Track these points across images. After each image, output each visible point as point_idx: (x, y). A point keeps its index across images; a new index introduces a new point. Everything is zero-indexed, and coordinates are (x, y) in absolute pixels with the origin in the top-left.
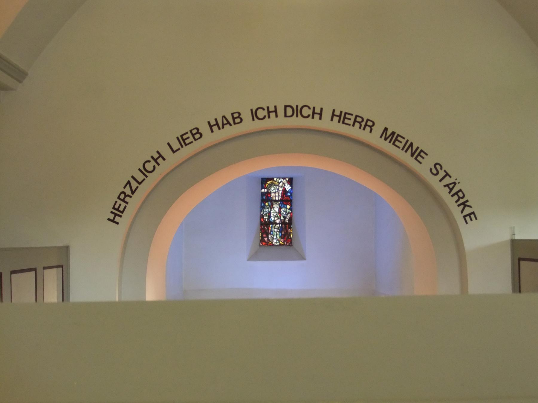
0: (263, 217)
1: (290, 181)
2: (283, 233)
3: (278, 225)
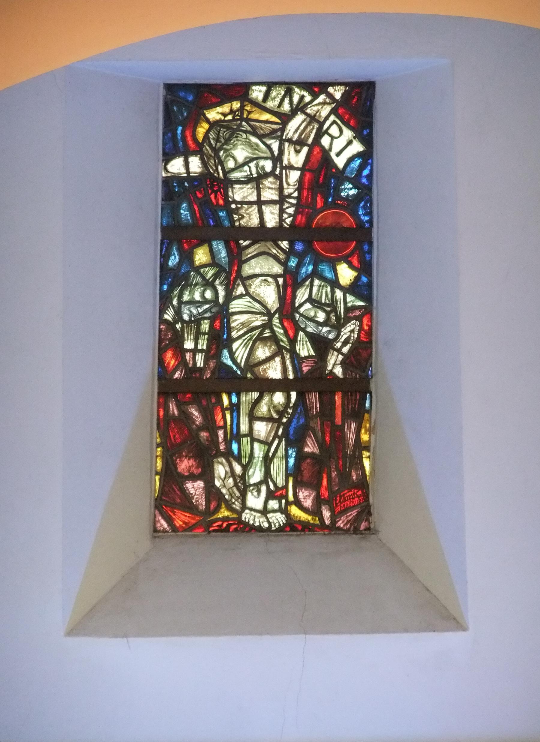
0: (177, 340)
1: (359, 105)
2: (311, 447)
3: (279, 398)
